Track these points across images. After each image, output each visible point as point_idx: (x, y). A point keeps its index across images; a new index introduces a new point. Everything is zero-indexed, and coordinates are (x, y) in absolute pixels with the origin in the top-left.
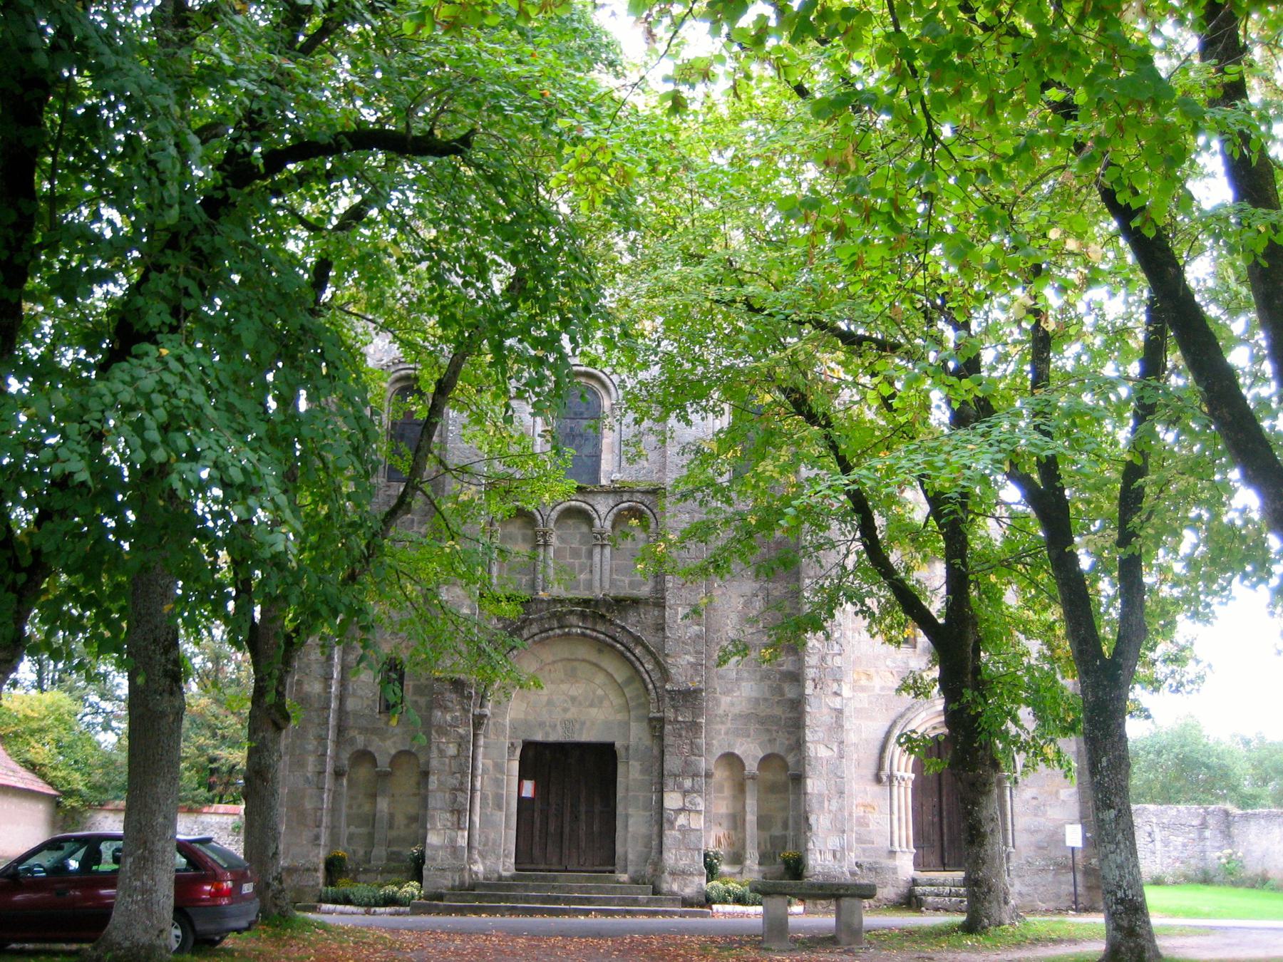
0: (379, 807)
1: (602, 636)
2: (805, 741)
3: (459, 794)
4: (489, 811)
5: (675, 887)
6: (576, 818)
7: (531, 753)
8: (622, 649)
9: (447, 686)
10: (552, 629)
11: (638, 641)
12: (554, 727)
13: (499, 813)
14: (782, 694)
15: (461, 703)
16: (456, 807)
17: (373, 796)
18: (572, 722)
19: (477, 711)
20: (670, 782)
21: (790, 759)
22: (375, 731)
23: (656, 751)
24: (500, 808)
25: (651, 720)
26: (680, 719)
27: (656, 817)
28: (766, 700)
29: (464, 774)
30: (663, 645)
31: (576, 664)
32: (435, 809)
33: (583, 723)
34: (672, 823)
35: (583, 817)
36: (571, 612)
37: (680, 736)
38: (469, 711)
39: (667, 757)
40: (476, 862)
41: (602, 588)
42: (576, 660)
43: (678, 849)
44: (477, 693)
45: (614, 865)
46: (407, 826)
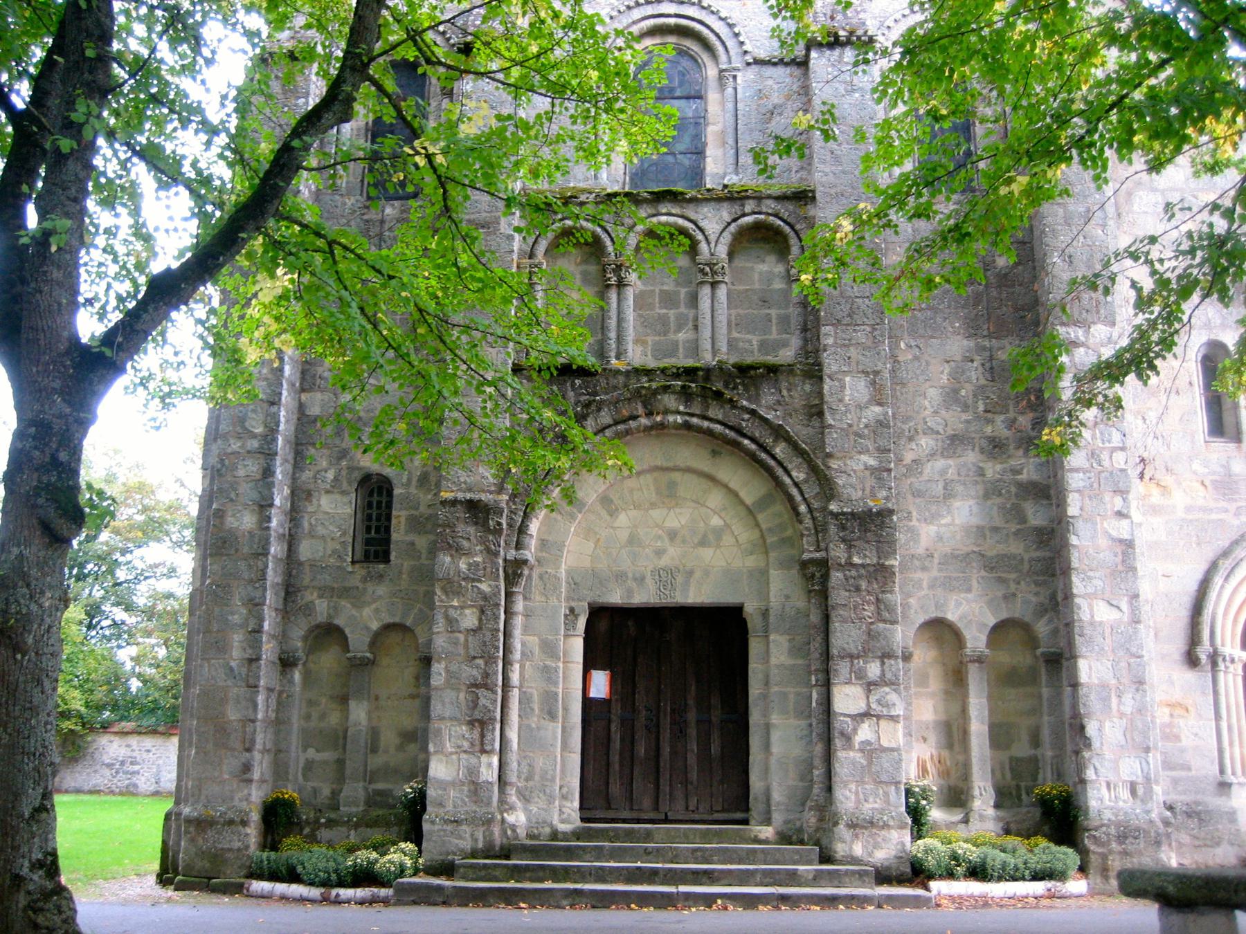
0: (352, 717)
1: (718, 428)
3: (482, 692)
4: (533, 722)
5: (858, 850)
6: (680, 732)
7: (603, 625)
8: (753, 447)
9: (460, 512)
10: (634, 418)
11: (779, 433)
12: (641, 580)
14: (1023, 520)
15: (483, 541)
16: (477, 715)
17: (343, 700)
18: (671, 572)
19: (512, 554)
20: (842, 668)
21: (1042, 628)
22: (345, 592)
23: (815, 617)
24: (552, 716)
25: (804, 565)
26: (856, 560)
27: (818, 728)
29: (491, 660)
31: (676, 476)
32: (442, 719)
33: (690, 573)
34: (848, 738)
35: (692, 732)
36: (666, 389)
37: (858, 589)
38: (496, 554)
39: (836, 625)
40: (512, 808)
41: (715, 352)
43: (861, 782)
44: (510, 526)
45: (747, 810)
46: (400, 748)
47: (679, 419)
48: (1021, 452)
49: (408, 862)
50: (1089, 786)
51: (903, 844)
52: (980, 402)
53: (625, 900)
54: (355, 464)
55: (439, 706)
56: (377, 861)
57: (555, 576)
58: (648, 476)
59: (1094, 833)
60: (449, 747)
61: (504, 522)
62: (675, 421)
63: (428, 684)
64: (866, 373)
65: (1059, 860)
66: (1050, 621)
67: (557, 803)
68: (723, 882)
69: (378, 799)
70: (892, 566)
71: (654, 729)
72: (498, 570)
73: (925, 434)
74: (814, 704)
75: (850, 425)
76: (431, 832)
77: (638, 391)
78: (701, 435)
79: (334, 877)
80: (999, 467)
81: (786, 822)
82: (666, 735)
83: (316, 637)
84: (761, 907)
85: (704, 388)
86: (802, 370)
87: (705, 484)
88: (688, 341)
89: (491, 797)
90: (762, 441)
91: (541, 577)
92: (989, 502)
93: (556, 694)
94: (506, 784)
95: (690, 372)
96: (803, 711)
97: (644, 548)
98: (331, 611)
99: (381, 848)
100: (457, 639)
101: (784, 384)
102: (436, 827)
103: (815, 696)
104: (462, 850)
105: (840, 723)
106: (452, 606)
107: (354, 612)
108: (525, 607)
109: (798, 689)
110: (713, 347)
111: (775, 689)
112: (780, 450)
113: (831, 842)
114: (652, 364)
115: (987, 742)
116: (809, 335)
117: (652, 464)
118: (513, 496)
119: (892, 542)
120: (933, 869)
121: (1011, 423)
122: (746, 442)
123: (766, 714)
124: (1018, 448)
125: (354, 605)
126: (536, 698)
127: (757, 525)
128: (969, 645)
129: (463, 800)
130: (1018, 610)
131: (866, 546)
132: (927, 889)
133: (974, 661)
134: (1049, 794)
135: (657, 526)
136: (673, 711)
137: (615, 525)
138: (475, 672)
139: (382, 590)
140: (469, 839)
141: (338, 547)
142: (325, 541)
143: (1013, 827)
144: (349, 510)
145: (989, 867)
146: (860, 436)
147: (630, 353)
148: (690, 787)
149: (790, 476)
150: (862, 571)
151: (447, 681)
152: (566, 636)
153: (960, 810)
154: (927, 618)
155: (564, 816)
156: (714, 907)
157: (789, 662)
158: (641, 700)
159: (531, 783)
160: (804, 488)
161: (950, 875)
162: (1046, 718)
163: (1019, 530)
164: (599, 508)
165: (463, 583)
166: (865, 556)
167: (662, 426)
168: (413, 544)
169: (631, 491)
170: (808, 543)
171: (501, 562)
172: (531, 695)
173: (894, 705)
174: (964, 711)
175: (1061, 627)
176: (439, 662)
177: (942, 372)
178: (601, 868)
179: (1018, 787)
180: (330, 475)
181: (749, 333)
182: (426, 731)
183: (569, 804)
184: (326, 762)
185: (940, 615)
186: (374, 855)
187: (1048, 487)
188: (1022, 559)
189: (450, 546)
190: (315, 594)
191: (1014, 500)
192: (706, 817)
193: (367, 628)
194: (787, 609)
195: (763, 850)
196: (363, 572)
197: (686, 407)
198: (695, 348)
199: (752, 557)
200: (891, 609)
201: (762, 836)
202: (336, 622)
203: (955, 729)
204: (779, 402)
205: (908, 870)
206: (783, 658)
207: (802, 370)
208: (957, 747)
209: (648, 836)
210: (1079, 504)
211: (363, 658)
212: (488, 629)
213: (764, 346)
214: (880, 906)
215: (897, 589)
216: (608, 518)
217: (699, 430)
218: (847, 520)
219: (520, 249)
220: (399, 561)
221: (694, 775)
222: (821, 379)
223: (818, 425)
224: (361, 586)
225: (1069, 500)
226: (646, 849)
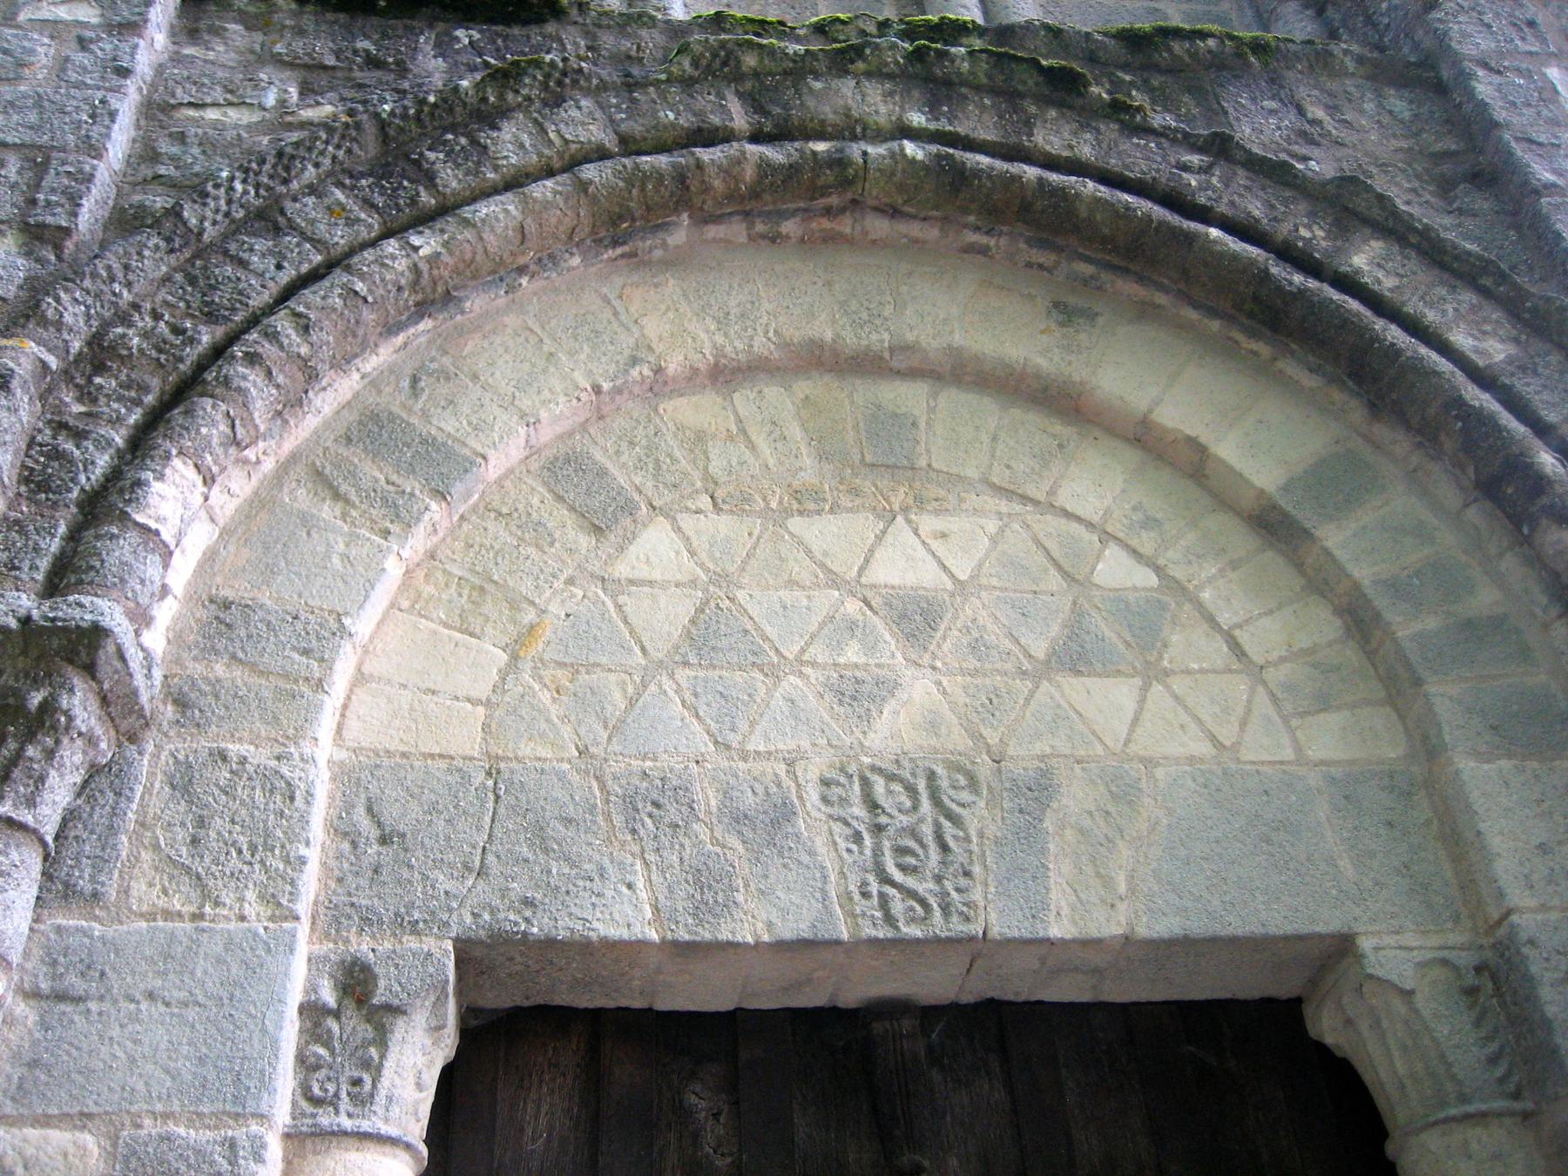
31: (910, 397)
57: (270, 781)
87: (1033, 427)
91: (183, 782)
97: (773, 674)
117: (795, 334)
137: (622, 570)
160: (1527, 387)
164: (537, 499)
197: (933, 109)
207: (1360, 60)
216: (585, 541)
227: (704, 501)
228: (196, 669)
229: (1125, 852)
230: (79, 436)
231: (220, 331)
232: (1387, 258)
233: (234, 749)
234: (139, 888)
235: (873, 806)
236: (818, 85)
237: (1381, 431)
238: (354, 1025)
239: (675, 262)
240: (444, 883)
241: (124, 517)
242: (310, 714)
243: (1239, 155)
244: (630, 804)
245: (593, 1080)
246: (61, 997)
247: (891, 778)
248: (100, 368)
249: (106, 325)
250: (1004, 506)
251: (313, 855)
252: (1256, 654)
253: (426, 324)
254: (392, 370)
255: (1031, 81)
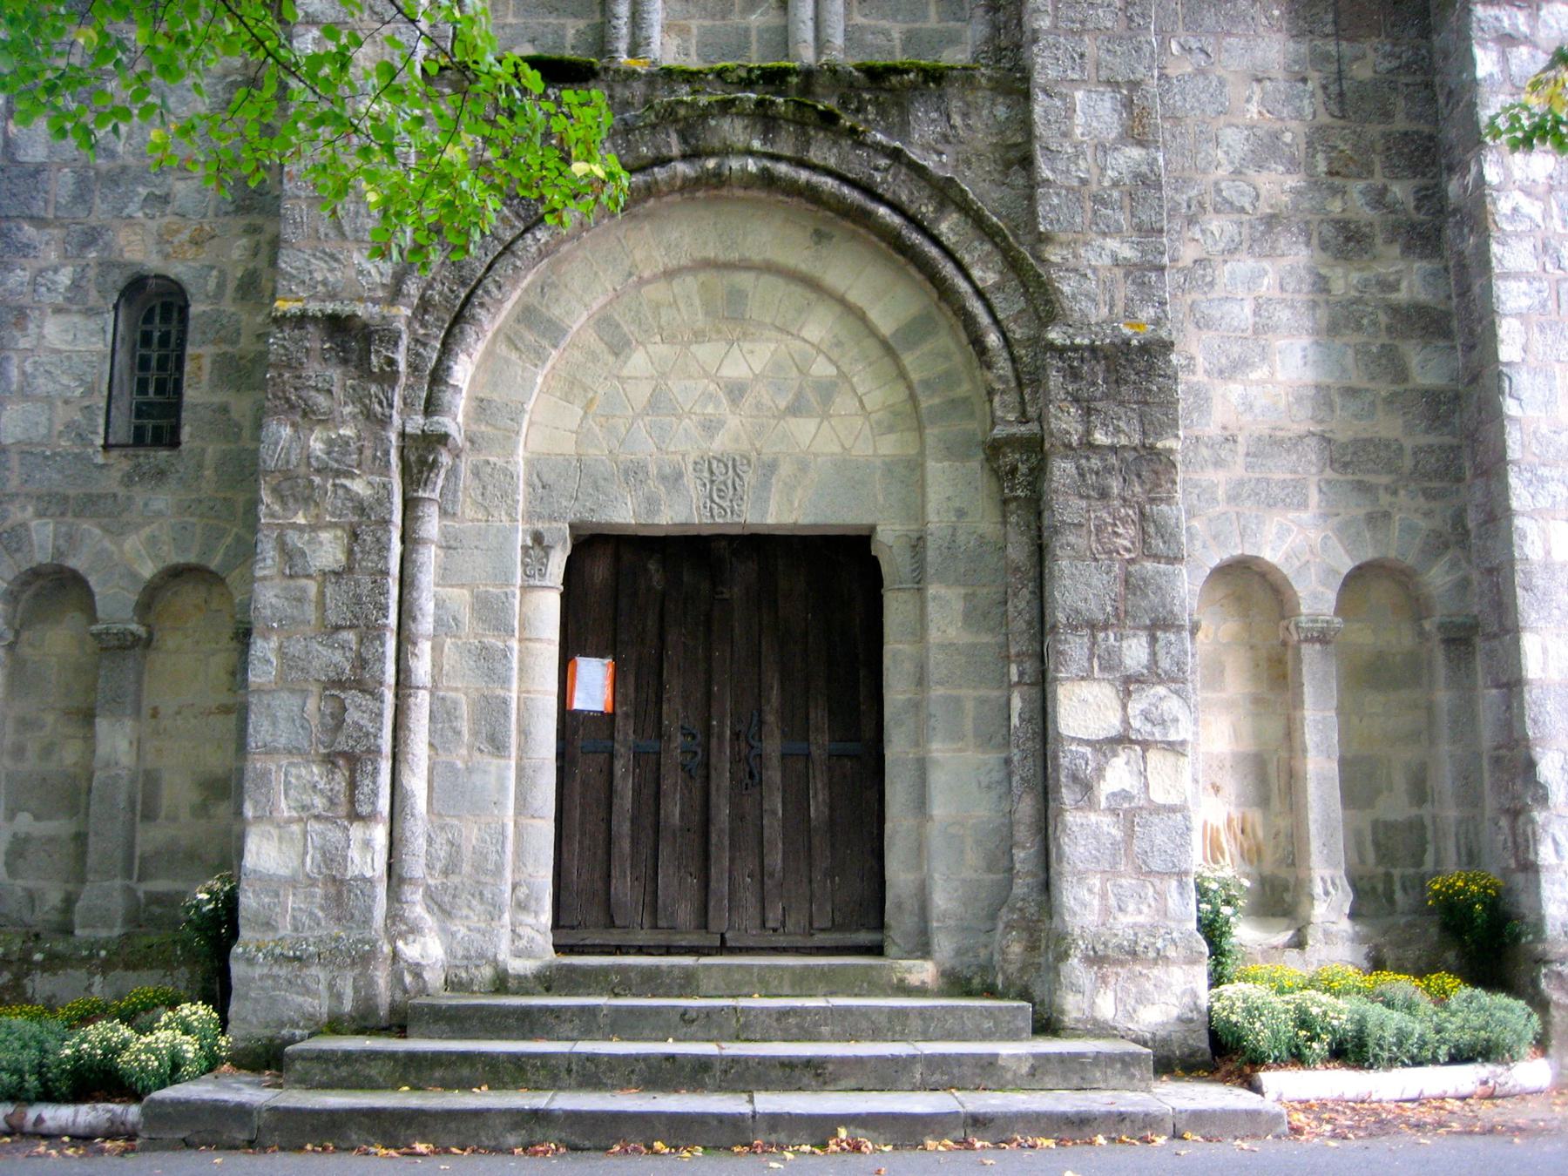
0: (103, 749)
1: (829, 183)
2: (1508, 513)
3: (352, 697)
4: (459, 757)
5: (1106, 1007)
6: (750, 777)
7: (599, 570)
8: (896, 220)
9: (314, 339)
10: (663, 161)
11: (946, 193)
12: (673, 479)
13: (494, 764)
14: (1401, 374)
15: (358, 397)
16: (343, 744)
17: (87, 717)
18: (733, 464)
19: (417, 423)
20: (1074, 648)
21: (1437, 578)
22: (89, 505)
23: (1018, 551)
24: (497, 745)
25: (994, 449)
26: (1100, 438)
27: (1024, 769)
28: (1350, 392)
29: (371, 632)
30: (1032, 213)
31: (745, 280)
32: (270, 751)
33: (771, 467)
34: (1087, 788)
35: (774, 775)
36: (726, 106)
37: (1104, 494)
38: (385, 422)
39: (1063, 565)
40: (414, 930)
41: (820, 44)
42: (745, 266)
43: (1112, 873)
44: (414, 368)
45: (881, 926)
46: (202, 810)
47: (752, 165)
48: (1396, 250)
49: (190, 1047)
50: (1544, 878)
51: (1195, 995)
52: (1320, 156)
53: (644, 1129)
54: (114, 256)
55: (266, 725)
56: (125, 1044)
58: (689, 279)
59: (1557, 967)
60: (285, 809)
61: (401, 358)
62: (744, 169)
63: (245, 683)
64: (1113, 84)
65: (1501, 1022)
66: (1454, 565)
67: (506, 917)
68: (843, 1084)
69: (157, 910)
70: (1171, 451)
71: (700, 772)
72: (387, 453)
73: (1217, 211)
74: (1015, 721)
75: (1084, 182)
76: (248, 981)
77: (671, 110)
78: (795, 200)
79: (32, 1081)
80: (1355, 277)
81: (959, 952)
82: (722, 779)
83: (37, 595)
84: (930, 1143)
85: (800, 105)
86: (990, 79)
88: (767, 30)
89: (370, 909)
90: (912, 209)
91: (476, 473)
92: (1338, 342)
93: (505, 702)
94: (402, 880)
95: (774, 78)
96: (995, 732)
98: (61, 542)
99: (138, 1016)
100: (304, 590)
101: (955, 105)
102: (258, 971)
103: (1017, 703)
104: (311, 1017)
105: (1070, 757)
106: (294, 526)
107: (107, 543)
108: (444, 532)
109: (983, 692)
110: (817, 38)
111: (937, 692)
112: (948, 227)
113: (1052, 992)
114: (694, 64)
115: (1338, 794)
116: (1001, 17)
117: (698, 255)
118: (425, 305)
119: (1170, 404)
120: (1264, 1046)
121: (1379, 198)
122: (882, 211)
123: (920, 739)
124: (1390, 241)
125: (106, 530)
126: (464, 710)
127: (902, 375)
128: (1304, 609)
129: (311, 914)
130: (1394, 545)
131: (1121, 411)
132: (1255, 1088)
133: (1311, 640)
134: (1461, 891)
135: (707, 375)
136: (736, 735)
137: (625, 373)
138: (338, 657)
139: (162, 500)
140: (325, 994)
141: (78, 417)
142: (52, 406)
143: (1388, 954)
144: (101, 345)
145: (1371, 1042)
146: (1104, 203)
147: (656, 45)
148: (768, 882)
149: (968, 277)
150: (1113, 460)
151: (282, 676)
152: (526, 589)
153: (1285, 921)
154: (1225, 556)
155: (522, 944)
156: (833, 1147)
157: (966, 638)
158: (674, 714)
159: (455, 880)
160: (997, 300)
161: (1297, 1058)
162: (1444, 748)
163: (1395, 394)
165: (317, 480)
166: (1118, 430)
167: (717, 180)
168: (224, 409)
169: (657, 307)
170: (1004, 405)
171: (393, 437)
172: (455, 702)
173: (1176, 720)
174: (1291, 735)
175: (1475, 576)
176: (266, 639)
177: (1248, 100)
178: (592, 1058)
179: (1388, 877)
180: (65, 278)
181: (884, 17)
182: (241, 772)
183: (530, 919)
184: (51, 840)
185: (1250, 551)
186: (126, 1032)
187: (1447, 315)
188: (1401, 448)
189: (292, 407)
190: (30, 509)
191: (1384, 339)
192: (799, 941)
193: (134, 576)
194: (961, 538)
195: (921, 1012)
196: (126, 465)
197: (765, 141)
198: (783, 38)
199: (893, 437)
200: (1168, 534)
201: (914, 979)
202: (72, 563)
203: (1272, 769)
204: (945, 137)
205: (1204, 1044)
206: (952, 633)
207: (990, 79)
208: (1276, 803)
209: (687, 983)
210: (1520, 340)
211: (120, 636)
212: (364, 570)
213: (910, 39)
214: (1177, 1135)
215: (1179, 496)
216: (611, 359)
217: (793, 190)
218: (1082, 360)
219: (514, 288)
220: (198, 443)
221: (775, 859)
222: (1027, 96)
223: (1021, 181)
224: (122, 492)
225: (1502, 332)
226: (684, 1012)
227: (658, 338)
228: (474, 427)
229: (799, 492)
230: (425, 345)
231: (467, 290)
232: (957, 225)
233: (492, 459)
234: (467, 511)
235: (712, 472)
236: (713, 123)
237: (943, 305)
238: (538, 552)
239: (649, 215)
240: (564, 503)
241: (446, 383)
242: (516, 444)
243: (905, 160)
244: (626, 472)
245: (617, 558)
246: (449, 548)
247: (719, 461)
248: (426, 311)
249: (425, 290)
250: (779, 336)
251: (520, 498)
252: (868, 407)
253: (546, 261)
254: (533, 283)
255: (813, 117)
